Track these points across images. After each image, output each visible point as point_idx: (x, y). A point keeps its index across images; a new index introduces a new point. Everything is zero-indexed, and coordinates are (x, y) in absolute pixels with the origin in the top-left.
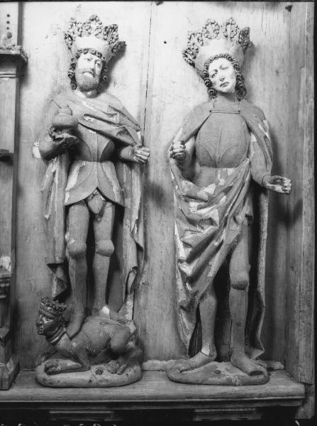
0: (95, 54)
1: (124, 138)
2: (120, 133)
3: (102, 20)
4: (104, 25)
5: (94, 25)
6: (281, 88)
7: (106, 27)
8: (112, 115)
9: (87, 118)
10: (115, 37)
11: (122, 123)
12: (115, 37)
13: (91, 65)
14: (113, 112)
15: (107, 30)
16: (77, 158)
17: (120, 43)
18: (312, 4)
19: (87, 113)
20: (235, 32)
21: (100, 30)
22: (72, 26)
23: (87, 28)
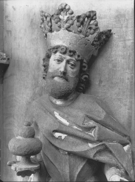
0: (65, 53)
1: (104, 158)
2: (99, 152)
3: (73, 8)
4: (76, 14)
5: (64, 17)
6: (54, 141)
7: (79, 17)
8: (89, 129)
9: (57, 135)
10: (94, 27)
11: (102, 138)
12: (94, 27)
13: (62, 67)
14: (92, 123)
15: (81, 19)
16: (96, 176)
17: (102, 33)
18: (1, 1)
19: (55, 129)
20: (92, 31)
21: (71, 22)
22: (43, 21)
23: (56, 20)
